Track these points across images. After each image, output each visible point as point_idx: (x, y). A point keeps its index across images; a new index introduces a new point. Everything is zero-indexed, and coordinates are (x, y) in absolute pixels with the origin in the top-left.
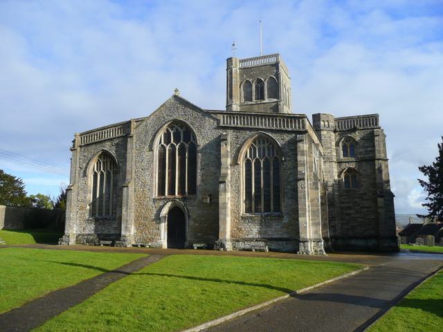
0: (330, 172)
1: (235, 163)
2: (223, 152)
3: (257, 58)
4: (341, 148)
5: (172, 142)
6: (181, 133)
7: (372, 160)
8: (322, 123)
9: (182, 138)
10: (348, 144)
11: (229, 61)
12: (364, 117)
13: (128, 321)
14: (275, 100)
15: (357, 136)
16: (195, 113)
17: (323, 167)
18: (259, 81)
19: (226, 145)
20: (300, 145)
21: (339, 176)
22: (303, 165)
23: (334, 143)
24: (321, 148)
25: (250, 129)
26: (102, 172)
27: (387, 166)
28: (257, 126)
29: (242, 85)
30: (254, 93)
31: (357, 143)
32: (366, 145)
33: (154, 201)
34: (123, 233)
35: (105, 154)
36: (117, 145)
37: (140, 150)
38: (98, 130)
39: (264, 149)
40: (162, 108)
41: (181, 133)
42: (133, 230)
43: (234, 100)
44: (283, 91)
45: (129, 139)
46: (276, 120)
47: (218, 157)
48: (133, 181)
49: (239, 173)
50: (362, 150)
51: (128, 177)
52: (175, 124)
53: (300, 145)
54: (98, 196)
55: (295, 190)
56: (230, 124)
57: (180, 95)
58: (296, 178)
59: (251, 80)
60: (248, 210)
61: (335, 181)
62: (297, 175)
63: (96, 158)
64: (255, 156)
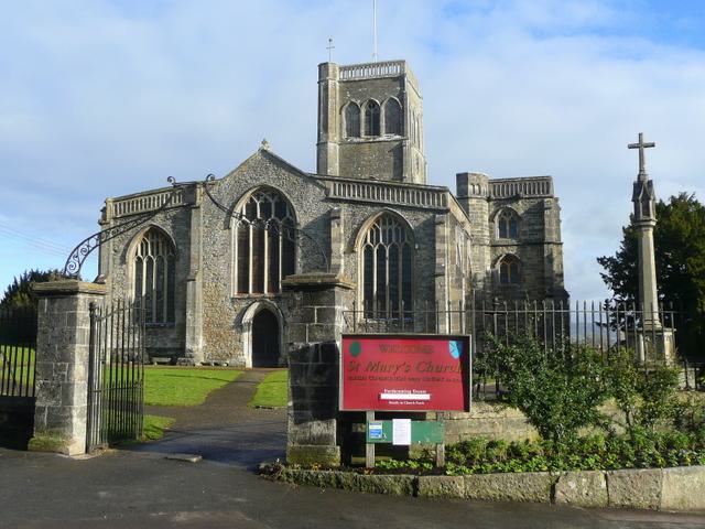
0: (480, 260)
1: (351, 250)
2: (334, 234)
3: (378, 65)
4: (497, 224)
5: (259, 216)
6: (272, 209)
7: (540, 243)
8: (470, 187)
9: (273, 212)
10: (507, 219)
11: (323, 68)
12: (531, 179)
13: (542, 348)
14: (398, 137)
15: (520, 208)
16: (293, 178)
17: (469, 252)
18: (372, 104)
19: (338, 225)
20: (439, 228)
21: (493, 266)
22: (443, 255)
23: (486, 217)
24: (468, 228)
25: (373, 204)
26: (150, 259)
27: (560, 253)
28: (381, 201)
29: (344, 109)
30: (363, 125)
31: (520, 218)
32: (533, 221)
33: (233, 302)
34: (188, 346)
35: (155, 232)
36: (174, 219)
37: (210, 226)
38: (142, 195)
39: (390, 231)
40: (244, 168)
41: (272, 209)
42: (202, 342)
43: (330, 135)
44: (410, 120)
45: (193, 211)
46: (408, 193)
47: (327, 242)
48: (200, 273)
49: (356, 263)
50: (526, 229)
51: (193, 266)
52: (263, 190)
53: (439, 228)
54: (144, 293)
55: (432, 289)
56: (344, 195)
57: (270, 150)
58: (433, 273)
59: (358, 102)
60: (368, 314)
61: (487, 273)
62: (435, 268)
63: (140, 237)
64: (378, 241)
